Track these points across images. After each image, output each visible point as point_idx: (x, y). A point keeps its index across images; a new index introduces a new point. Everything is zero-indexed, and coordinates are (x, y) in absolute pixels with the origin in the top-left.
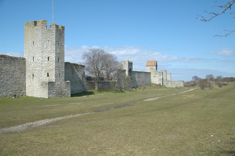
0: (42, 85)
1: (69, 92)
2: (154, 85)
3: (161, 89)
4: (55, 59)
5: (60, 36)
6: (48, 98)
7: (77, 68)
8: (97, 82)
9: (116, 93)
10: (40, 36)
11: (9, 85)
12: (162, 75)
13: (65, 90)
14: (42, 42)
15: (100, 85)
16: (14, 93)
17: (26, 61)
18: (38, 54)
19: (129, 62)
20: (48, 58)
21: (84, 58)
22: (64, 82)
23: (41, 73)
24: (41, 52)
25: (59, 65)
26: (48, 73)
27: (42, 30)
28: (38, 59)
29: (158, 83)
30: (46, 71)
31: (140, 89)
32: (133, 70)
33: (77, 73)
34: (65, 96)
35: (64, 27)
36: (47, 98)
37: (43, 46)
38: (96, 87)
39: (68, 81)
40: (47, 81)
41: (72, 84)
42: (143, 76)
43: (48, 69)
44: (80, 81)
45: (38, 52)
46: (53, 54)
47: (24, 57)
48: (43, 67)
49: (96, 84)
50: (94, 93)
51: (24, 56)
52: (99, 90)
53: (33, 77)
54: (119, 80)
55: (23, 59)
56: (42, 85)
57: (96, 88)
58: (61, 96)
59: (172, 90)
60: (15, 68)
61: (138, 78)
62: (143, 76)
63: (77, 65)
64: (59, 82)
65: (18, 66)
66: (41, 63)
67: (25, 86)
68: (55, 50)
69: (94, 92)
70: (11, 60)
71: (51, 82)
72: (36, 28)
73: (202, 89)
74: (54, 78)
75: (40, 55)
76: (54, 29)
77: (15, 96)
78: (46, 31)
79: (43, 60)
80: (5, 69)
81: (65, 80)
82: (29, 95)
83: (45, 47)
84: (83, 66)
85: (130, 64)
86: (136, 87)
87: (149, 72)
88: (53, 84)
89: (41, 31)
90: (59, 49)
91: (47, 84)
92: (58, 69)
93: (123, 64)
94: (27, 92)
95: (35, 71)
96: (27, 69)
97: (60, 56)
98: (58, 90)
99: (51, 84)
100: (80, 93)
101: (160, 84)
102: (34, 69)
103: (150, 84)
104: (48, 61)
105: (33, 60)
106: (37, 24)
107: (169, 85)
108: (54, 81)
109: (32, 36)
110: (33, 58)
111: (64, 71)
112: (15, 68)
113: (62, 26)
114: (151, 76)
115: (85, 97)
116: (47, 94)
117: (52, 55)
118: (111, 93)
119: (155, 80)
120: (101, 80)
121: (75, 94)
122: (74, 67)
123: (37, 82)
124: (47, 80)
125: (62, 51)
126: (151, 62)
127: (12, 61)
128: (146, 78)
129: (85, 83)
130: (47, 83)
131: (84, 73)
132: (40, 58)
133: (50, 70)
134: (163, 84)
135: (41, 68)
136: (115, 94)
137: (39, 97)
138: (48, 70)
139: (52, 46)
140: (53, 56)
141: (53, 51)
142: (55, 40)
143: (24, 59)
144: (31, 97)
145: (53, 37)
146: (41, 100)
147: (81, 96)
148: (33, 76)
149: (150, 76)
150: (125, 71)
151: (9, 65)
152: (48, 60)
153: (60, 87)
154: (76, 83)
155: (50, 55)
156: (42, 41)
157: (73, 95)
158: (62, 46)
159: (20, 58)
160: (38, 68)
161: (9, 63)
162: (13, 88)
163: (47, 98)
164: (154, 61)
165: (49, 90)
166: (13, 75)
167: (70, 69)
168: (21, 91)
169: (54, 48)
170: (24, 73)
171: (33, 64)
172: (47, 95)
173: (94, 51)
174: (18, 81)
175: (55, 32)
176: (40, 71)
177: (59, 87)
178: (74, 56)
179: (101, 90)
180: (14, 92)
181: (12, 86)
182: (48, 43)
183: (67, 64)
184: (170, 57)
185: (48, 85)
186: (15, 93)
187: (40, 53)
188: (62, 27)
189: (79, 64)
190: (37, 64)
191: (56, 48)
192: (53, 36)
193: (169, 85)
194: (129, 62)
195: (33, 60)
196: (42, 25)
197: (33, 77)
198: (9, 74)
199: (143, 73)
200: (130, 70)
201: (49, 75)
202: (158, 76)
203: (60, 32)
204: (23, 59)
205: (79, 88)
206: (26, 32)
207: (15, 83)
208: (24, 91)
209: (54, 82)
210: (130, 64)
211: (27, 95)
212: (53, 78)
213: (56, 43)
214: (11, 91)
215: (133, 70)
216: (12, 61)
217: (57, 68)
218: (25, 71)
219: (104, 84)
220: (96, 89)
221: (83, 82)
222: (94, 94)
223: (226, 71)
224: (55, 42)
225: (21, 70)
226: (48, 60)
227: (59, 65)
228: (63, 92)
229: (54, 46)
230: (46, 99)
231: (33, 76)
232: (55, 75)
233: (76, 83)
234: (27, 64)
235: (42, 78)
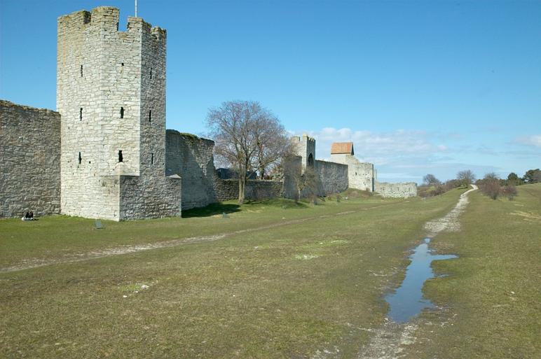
0: (104, 185)
1: (179, 203)
2: (356, 192)
3: (372, 201)
4: (139, 115)
5: (155, 52)
6: (121, 220)
7: (195, 147)
8: (243, 182)
9: (287, 208)
10: (100, 49)
11: (12, 184)
12: (371, 171)
13: (168, 198)
14: (104, 67)
15: (250, 189)
16: (24, 208)
17: (63, 121)
18: (94, 99)
19: (308, 138)
20: (122, 110)
21: (211, 124)
22: (163, 178)
23: (102, 152)
24: (101, 95)
25: (152, 130)
26: (120, 151)
27: (107, 33)
28: (95, 115)
29: (363, 188)
30: (114, 147)
31: (330, 199)
32: (317, 158)
33: (195, 159)
34: (167, 216)
35: (165, 31)
36: (117, 219)
37: (106, 77)
38: (240, 194)
39: (176, 176)
40: (119, 173)
41: (186, 184)
42: (334, 171)
43: (120, 141)
44: (202, 178)
45: (93, 95)
46: (134, 99)
47: (57, 111)
48: (106, 134)
49: (240, 186)
50: (239, 208)
51: (57, 106)
52: (247, 201)
53: (80, 163)
54: (288, 178)
55: (54, 116)
56: (104, 185)
57: (241, 196)
58: (156, 215)
59: (398, 203)
60: (30, 137)
61: (325, 176)
62: (334, 171)
63: (196, 137)
64: (151, 178)
65: (39, 131)
66: (101, 123)
67: (59, 190)
68: (140, 89)
69: (238, 206)
70: (17, 116)
71: (129, 178)
72: (89, 28)
73: (495, 198)
74: (138, 166)
75: (99, 102)
76: (137, 32)
77: (29, 215)
78: (115, 37)
79: (106, 115)
80: (10, 137)
81: (168, 173)
82: (68, 214)
83: (113, 79)
84: (210, 143)
85: (311, 143)
86: (323, 195)
87: (345, 163)
88: (135, 183)
89: (101, 37)
90: (152, 87)
91: (119, 182)
92: (149, 142)
93: (295, 142)
94: (62, 204)
95: (84, 148)
96: (65, 140)
97: (152, 111)
98: (147, 198)
99: (127, 180)
100: (204, 208)
101: (367, 190)
102: (81, 140)
103: (344, 189)
105: (81, 118)
106: (92, 19)
107: (386, 193)
108: (138, 175)
109: (77, 52)
110: (80, 110)
111: (164, 146)
112: (30, 137)
113: (159, 28)
114: (349, 172)
115: (217, 217)
116: (118, 208)
117: (133, 103)
118: (277, 209)
119: (357, 181)
120: (250, 178)
121: (190, 210)
122: (189, 143)
124: (118, 170)
125: (160, 94)
126: (342, 145)
127: (20, 118)
128: (339, 176)
129: (215, 183)
130: (119, 177)
131: (212, 159)
132: (99, 110)
133: (127, 144)
134: (373, 190)
135: (102, 139)
136: (287, 210)
137: (95, 217)
138: (121, 144)
139: (133, 77)
140: (135, 107)
142: (140, 63)
143: (55, 115)
144: (74, 217)
145: (134, 53)
146: (99, 225)
147: (208, 214)
148: (80, 159)
149: (347, 172)
150: (300, 158)
151: (12, 129)
152: (122, 117)
153: (153, 192)
154: (193, 183)
155: (126, 103)
156: (104, 64)
157: (186, 213)
158: (159, 79)
159: (46, 110)
160: (92, 139)
161: (11, 121)
162: (24, 192)
163: (117, 219)
164: (348, 144)
165: (122, 198)
166: (24, 156)
167: (181, 146)
168: (46, 200)
169: (137, 85)
170: (55, 151)
171: (79, 128)
172: (118, 213)
173: (236, 108)
174: (38, 173)
175: (140, 39)
176: (99, 146)
177: (150, 190)
178: (189, 117)
179: (252, 200)
180: (27, 203)
181: (21, 188)
182: (120, 68)
183: (171, 134)
184: (392, 135)
185: (121, 184)
186: (28, 206)
187: (98, 96)
188: (160, 30)
189: (199, 137)
190: (92, 127)
191: (143, 84)
192: (135, 51)
193: (386, 192)
194: (308, 138)
195: (81, 118)
196: (104, 20)
197: (80, 163)
198: (12, 152)
199: (335, 166)
200: (311, 158)
202: (363, 172)
203: (155, 45)
204: (54, 116)
205: (200, 197)
206: (62, 43)
207: (30, 180)
208: (54, 202)
209: (137, 177)
210: (311, 143)
211: (65, 211)
212: (133, 166)
213: (142, 72)
214: (18, 202)
215: (317, 158)
216: (20, 118)
217: (146, 137)
218: (59, 147)
219: (259, 191)
220: (240, 198)
221: (206, 182)
222: (239, 210)
223: (508, 163)
224: (140, 66)
225: (46, 143)
226: (122, 117)
227: (152, 130)
228: (162, 203)
229: (136, 79)
230: (113, 223)
231: (80, 159)
232: (141, 159)
233: (193, 183)
234: (64, 129)
235: (105, 165)
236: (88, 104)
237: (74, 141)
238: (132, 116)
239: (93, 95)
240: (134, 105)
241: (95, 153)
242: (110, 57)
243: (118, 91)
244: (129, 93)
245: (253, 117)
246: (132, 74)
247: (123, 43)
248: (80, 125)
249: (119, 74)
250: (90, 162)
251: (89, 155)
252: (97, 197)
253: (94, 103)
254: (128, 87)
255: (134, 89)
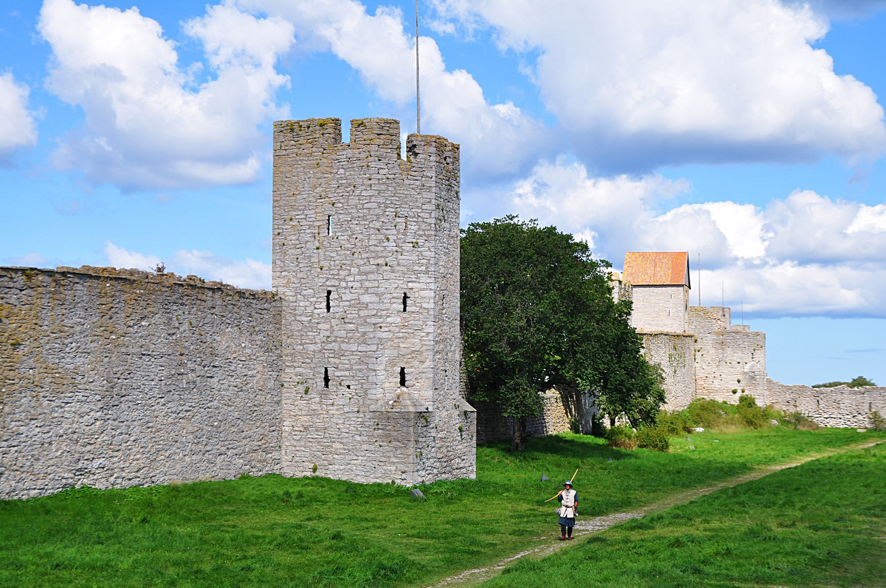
20: (405, 297)
30: (392, 363)
46: (424, 278)
53: (327, 386)
79: (381, 306)
104: (405, 315)
105: (328, 308)
123: (346, 409)
133: (415, 353)
141: (423, 268)
152: (405, 310)
192: (426, 195)
195: (328, 308)
196: (377, 141)
197: (327, 386)
199: (81, 289)
201: (407, 377)
224: (433, 221)
226: (405, 310)
231: (327, 380)
236: (343, 284)
237: (312, 347)
238: (421, 307)
239: (354, 270)
240: (424, 290)
241: (360, 370)
242: (387, 207)
243: (399, 265)
244: (416, 268)
245: (218, 72)
246: (420, 236)
247: (407, 182)
248: (326, 320)
249: (400, 236)
250: (349, 387)
251: (347, 373)
252: (365, 447)
253: (357, 285)
254: (415, 258)
255: (424, 261)
